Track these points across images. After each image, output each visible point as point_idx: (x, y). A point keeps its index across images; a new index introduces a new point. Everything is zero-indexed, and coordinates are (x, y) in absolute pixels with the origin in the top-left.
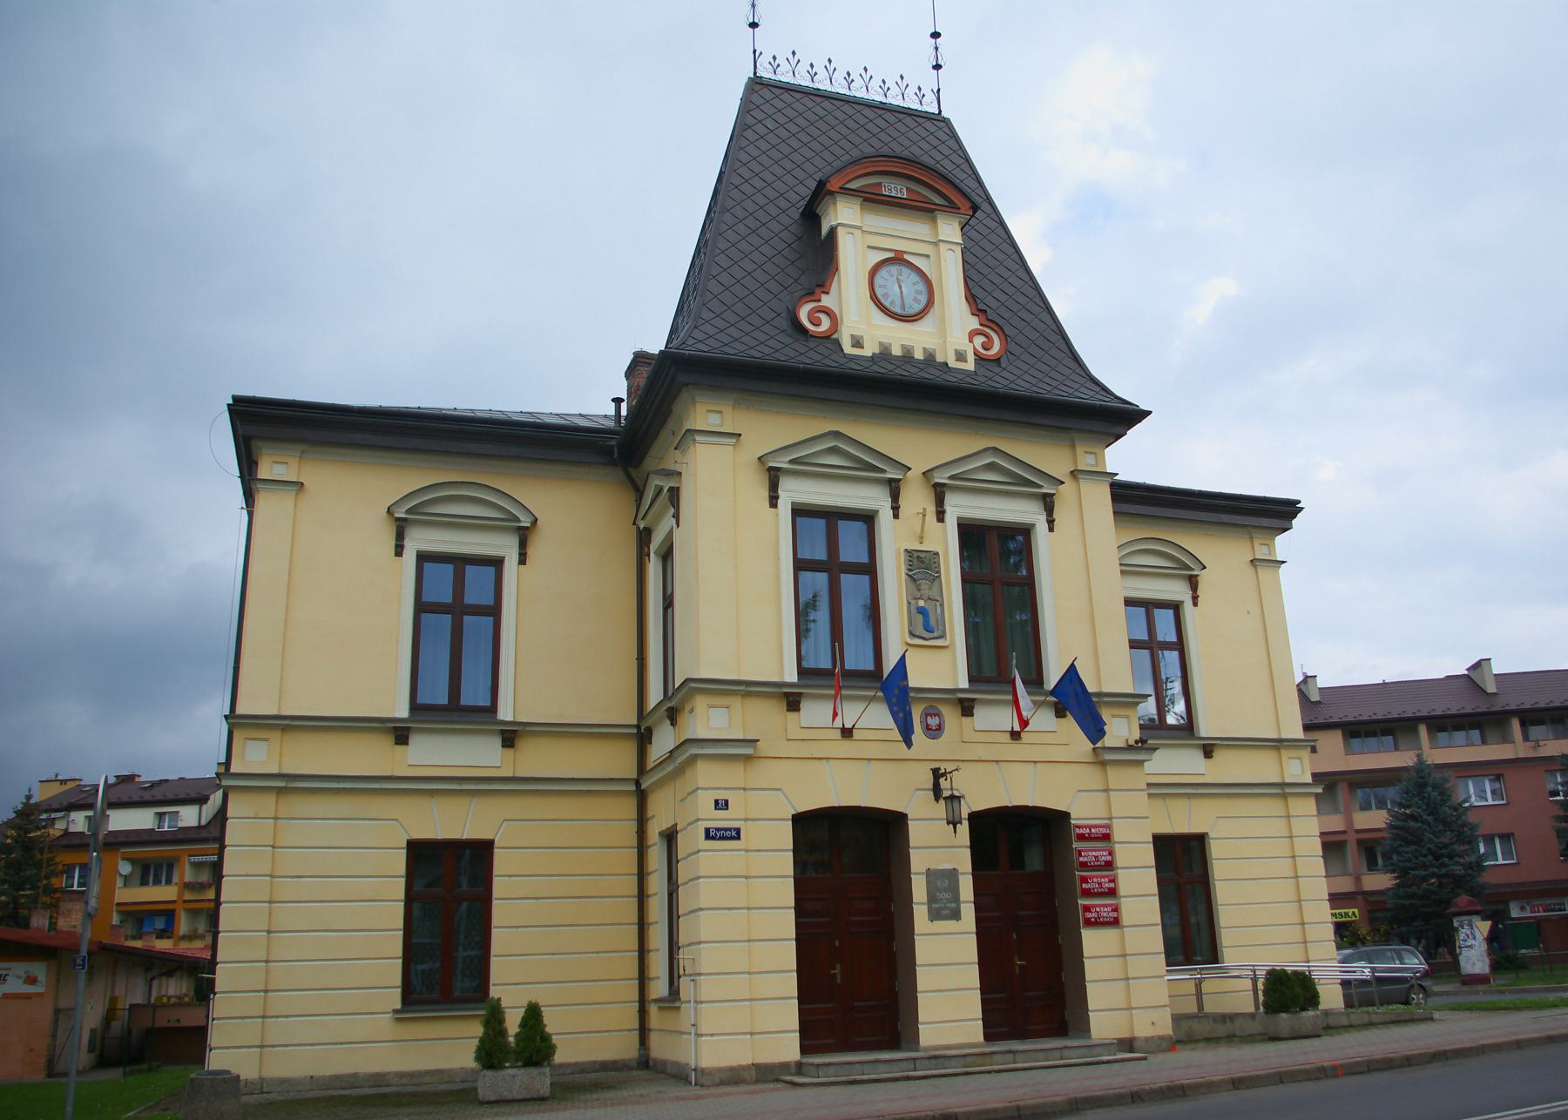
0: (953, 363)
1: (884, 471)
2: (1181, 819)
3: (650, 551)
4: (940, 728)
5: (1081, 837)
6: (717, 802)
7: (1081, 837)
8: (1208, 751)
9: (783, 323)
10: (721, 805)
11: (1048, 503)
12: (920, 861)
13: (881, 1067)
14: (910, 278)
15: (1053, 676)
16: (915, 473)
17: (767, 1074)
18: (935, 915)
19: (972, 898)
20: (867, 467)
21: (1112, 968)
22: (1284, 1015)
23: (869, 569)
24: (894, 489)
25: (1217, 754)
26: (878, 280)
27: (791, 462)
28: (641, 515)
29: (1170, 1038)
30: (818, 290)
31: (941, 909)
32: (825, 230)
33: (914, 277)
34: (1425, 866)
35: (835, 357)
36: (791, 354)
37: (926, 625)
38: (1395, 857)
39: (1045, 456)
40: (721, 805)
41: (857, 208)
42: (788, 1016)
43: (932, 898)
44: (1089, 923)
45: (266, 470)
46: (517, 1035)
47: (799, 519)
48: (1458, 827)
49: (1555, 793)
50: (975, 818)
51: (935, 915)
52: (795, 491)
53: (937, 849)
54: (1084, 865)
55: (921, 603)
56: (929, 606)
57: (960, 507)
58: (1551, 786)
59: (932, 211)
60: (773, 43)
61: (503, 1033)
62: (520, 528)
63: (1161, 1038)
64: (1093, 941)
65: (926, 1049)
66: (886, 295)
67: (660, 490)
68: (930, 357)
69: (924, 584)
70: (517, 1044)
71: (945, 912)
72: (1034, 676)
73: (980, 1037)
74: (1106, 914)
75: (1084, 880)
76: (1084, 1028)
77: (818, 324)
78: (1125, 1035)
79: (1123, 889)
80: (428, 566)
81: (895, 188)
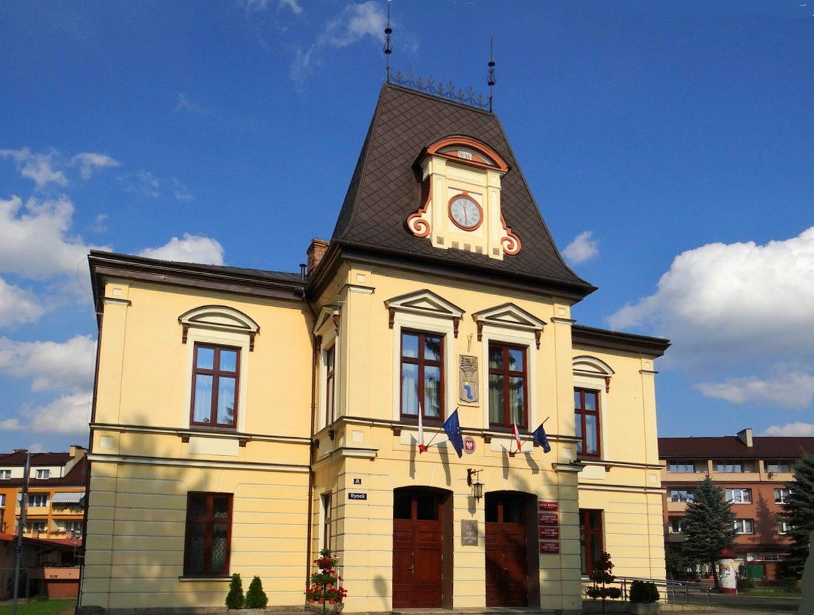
0: (492, 256)
3: (325, 350)
4: (473, 448)
5: (542, 508)
6: (355, 480)
7: (542, 508)
9: (402, 229)
11: (538, 333)
15: (533, 427)
18: (465, 543)
20: (443, 310)
23: (440, 364)
24: (456, 321)
25: (612, 469)
26: (453, 207)
27: (402, 305)
28: (316, 329)
31: (468, 540)
32: (425, 177)
33: (473, 206)
34: (704, 532)
35: (427, 248)
37: (469, 395)
38: (688, 527)
40: (357, 482)
43: (463, 534)
44: (544, 552)
45: (111, 290)
46: (248, 592)
47: (404, 336)
48: (727, 515)
49: (779, 500)
50: (487, 495)
51: (465, 543)
53: (467, 513)
54: (543, 523)
55: (467, 384)
57: (491, 333)
58: (777, 496)
59: (485, 169)
61: (241, 591)
62: (250, 333)
65: (457, 609)
66: (457, 215)
67: (327, 316)
70: (248, 596)
72: (523, 424)
74: (552, 547)
75: (542, 530)
78: (558, 608)
79: (562, 536)
80: (200, 350)
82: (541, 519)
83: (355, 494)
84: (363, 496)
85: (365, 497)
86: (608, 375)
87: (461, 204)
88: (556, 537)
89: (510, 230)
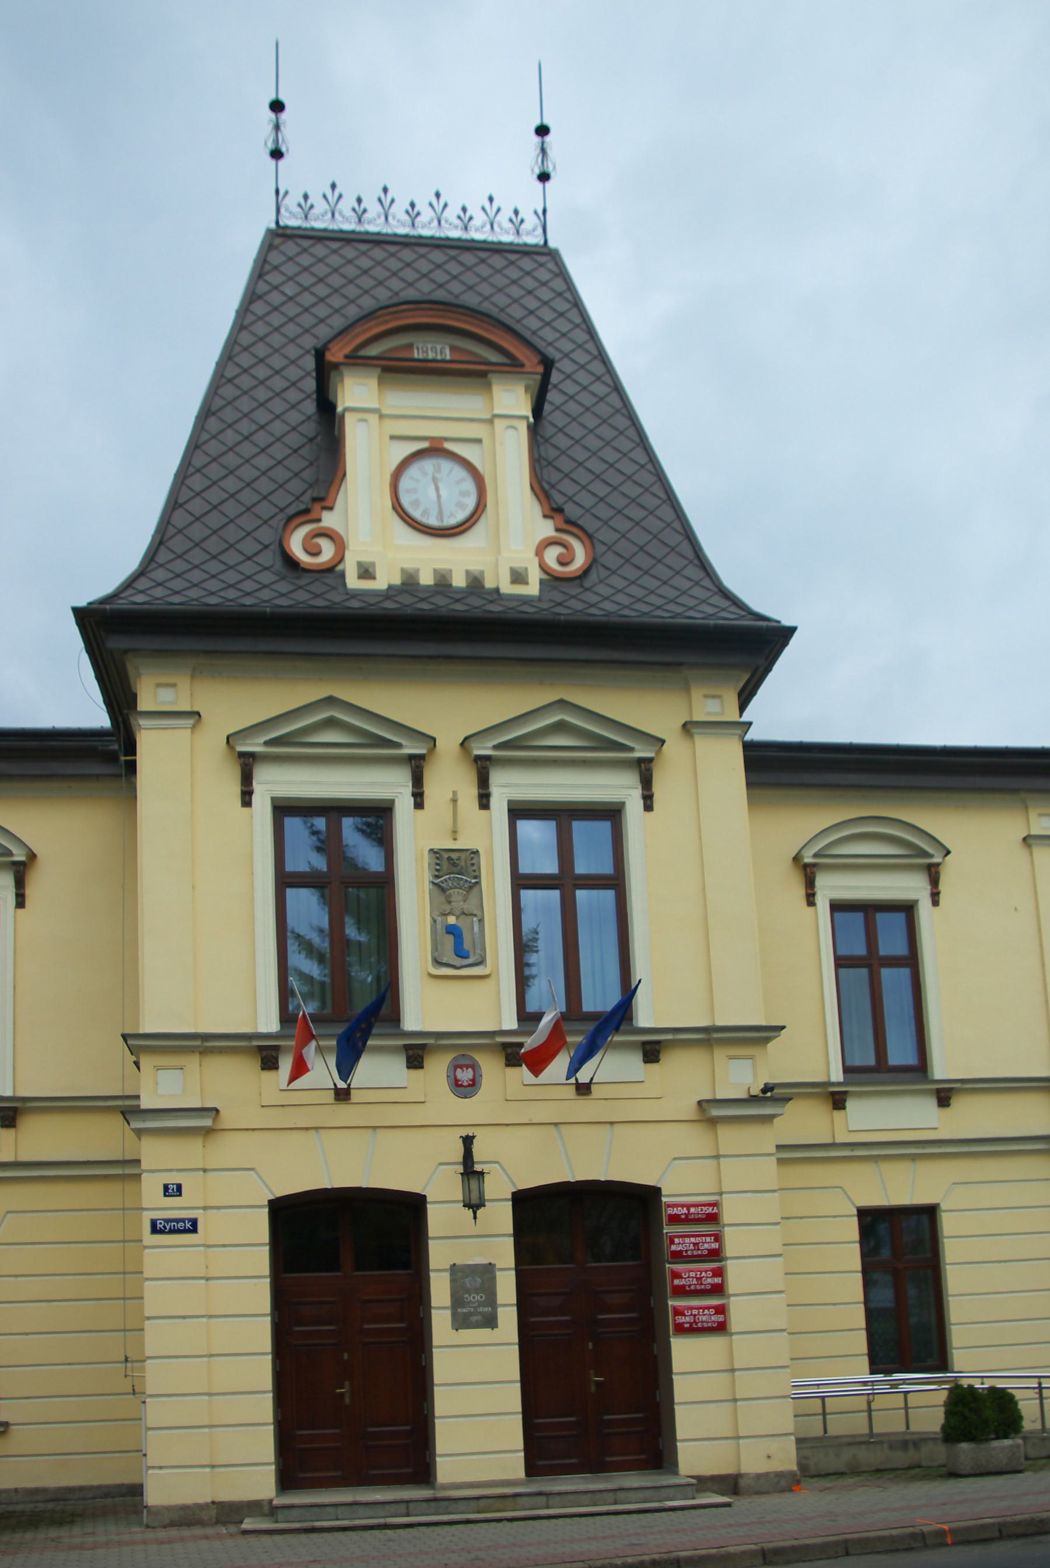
0: (507, 588)
1: (399, 746)
2: (898, 1187)
4: (474, 1084)
5: (674, 1219)
6: (166, 1188)
7: (674, 1219)
8: (944, 1097)
9: (268, 558)
10: (173, 1191)
12: (440, 1256)
13: (361, 1511)
14: (452, 475)
16: (448, 743)
17: (228, 1513)
18: (461, 1322)
19: (513, 1300)
20: (377, 743)
21: (717, 1386)
22: (964, 1445)
24: (417, 767)
26: (405, 483)
27: (267, 743)
29: (792, 1474)
30: (317, 507)
31: (471, 1314)
33: (459, 472)
36: (273, 594)
39: (644, 708)
40: (173, 1191)
41: (373, 383)
42: (263, 1444)
43: (457, 1301)
44: (681, 1330)
51: (461, 1322)
52: (276, 782)
53: (469, 1242)
54: (677, 1256)
55: (452, 920)
56: (463, 923)
59: (483, 375)
60: (302, 175)
63: (779, 1475)
64: (686, 1354)
66: (416, 503)
68: (475, 582)
69: (456, 895)
71: (474, 1319)
73: (521, 1473)
74: (709, 1318)
76: (674, 1464)
77: (317, 553)
81: (433, 349)
82: (673, 1248)
83: (168, 1221)
84: (188, 1225)
85: (193, 1227)
86: (935, 860)
87: (425, 474)
88: (718, 1290)
89: (559, 518)
